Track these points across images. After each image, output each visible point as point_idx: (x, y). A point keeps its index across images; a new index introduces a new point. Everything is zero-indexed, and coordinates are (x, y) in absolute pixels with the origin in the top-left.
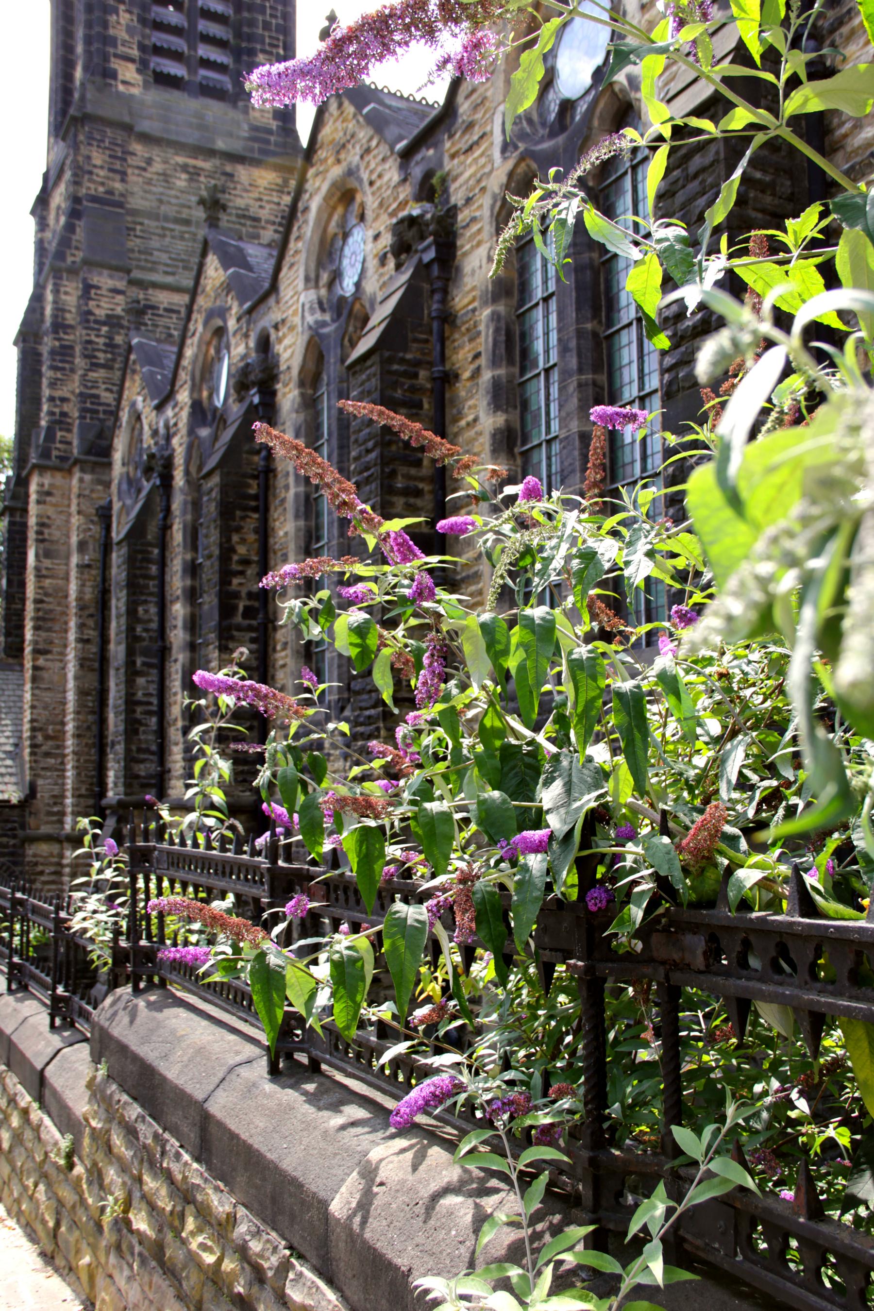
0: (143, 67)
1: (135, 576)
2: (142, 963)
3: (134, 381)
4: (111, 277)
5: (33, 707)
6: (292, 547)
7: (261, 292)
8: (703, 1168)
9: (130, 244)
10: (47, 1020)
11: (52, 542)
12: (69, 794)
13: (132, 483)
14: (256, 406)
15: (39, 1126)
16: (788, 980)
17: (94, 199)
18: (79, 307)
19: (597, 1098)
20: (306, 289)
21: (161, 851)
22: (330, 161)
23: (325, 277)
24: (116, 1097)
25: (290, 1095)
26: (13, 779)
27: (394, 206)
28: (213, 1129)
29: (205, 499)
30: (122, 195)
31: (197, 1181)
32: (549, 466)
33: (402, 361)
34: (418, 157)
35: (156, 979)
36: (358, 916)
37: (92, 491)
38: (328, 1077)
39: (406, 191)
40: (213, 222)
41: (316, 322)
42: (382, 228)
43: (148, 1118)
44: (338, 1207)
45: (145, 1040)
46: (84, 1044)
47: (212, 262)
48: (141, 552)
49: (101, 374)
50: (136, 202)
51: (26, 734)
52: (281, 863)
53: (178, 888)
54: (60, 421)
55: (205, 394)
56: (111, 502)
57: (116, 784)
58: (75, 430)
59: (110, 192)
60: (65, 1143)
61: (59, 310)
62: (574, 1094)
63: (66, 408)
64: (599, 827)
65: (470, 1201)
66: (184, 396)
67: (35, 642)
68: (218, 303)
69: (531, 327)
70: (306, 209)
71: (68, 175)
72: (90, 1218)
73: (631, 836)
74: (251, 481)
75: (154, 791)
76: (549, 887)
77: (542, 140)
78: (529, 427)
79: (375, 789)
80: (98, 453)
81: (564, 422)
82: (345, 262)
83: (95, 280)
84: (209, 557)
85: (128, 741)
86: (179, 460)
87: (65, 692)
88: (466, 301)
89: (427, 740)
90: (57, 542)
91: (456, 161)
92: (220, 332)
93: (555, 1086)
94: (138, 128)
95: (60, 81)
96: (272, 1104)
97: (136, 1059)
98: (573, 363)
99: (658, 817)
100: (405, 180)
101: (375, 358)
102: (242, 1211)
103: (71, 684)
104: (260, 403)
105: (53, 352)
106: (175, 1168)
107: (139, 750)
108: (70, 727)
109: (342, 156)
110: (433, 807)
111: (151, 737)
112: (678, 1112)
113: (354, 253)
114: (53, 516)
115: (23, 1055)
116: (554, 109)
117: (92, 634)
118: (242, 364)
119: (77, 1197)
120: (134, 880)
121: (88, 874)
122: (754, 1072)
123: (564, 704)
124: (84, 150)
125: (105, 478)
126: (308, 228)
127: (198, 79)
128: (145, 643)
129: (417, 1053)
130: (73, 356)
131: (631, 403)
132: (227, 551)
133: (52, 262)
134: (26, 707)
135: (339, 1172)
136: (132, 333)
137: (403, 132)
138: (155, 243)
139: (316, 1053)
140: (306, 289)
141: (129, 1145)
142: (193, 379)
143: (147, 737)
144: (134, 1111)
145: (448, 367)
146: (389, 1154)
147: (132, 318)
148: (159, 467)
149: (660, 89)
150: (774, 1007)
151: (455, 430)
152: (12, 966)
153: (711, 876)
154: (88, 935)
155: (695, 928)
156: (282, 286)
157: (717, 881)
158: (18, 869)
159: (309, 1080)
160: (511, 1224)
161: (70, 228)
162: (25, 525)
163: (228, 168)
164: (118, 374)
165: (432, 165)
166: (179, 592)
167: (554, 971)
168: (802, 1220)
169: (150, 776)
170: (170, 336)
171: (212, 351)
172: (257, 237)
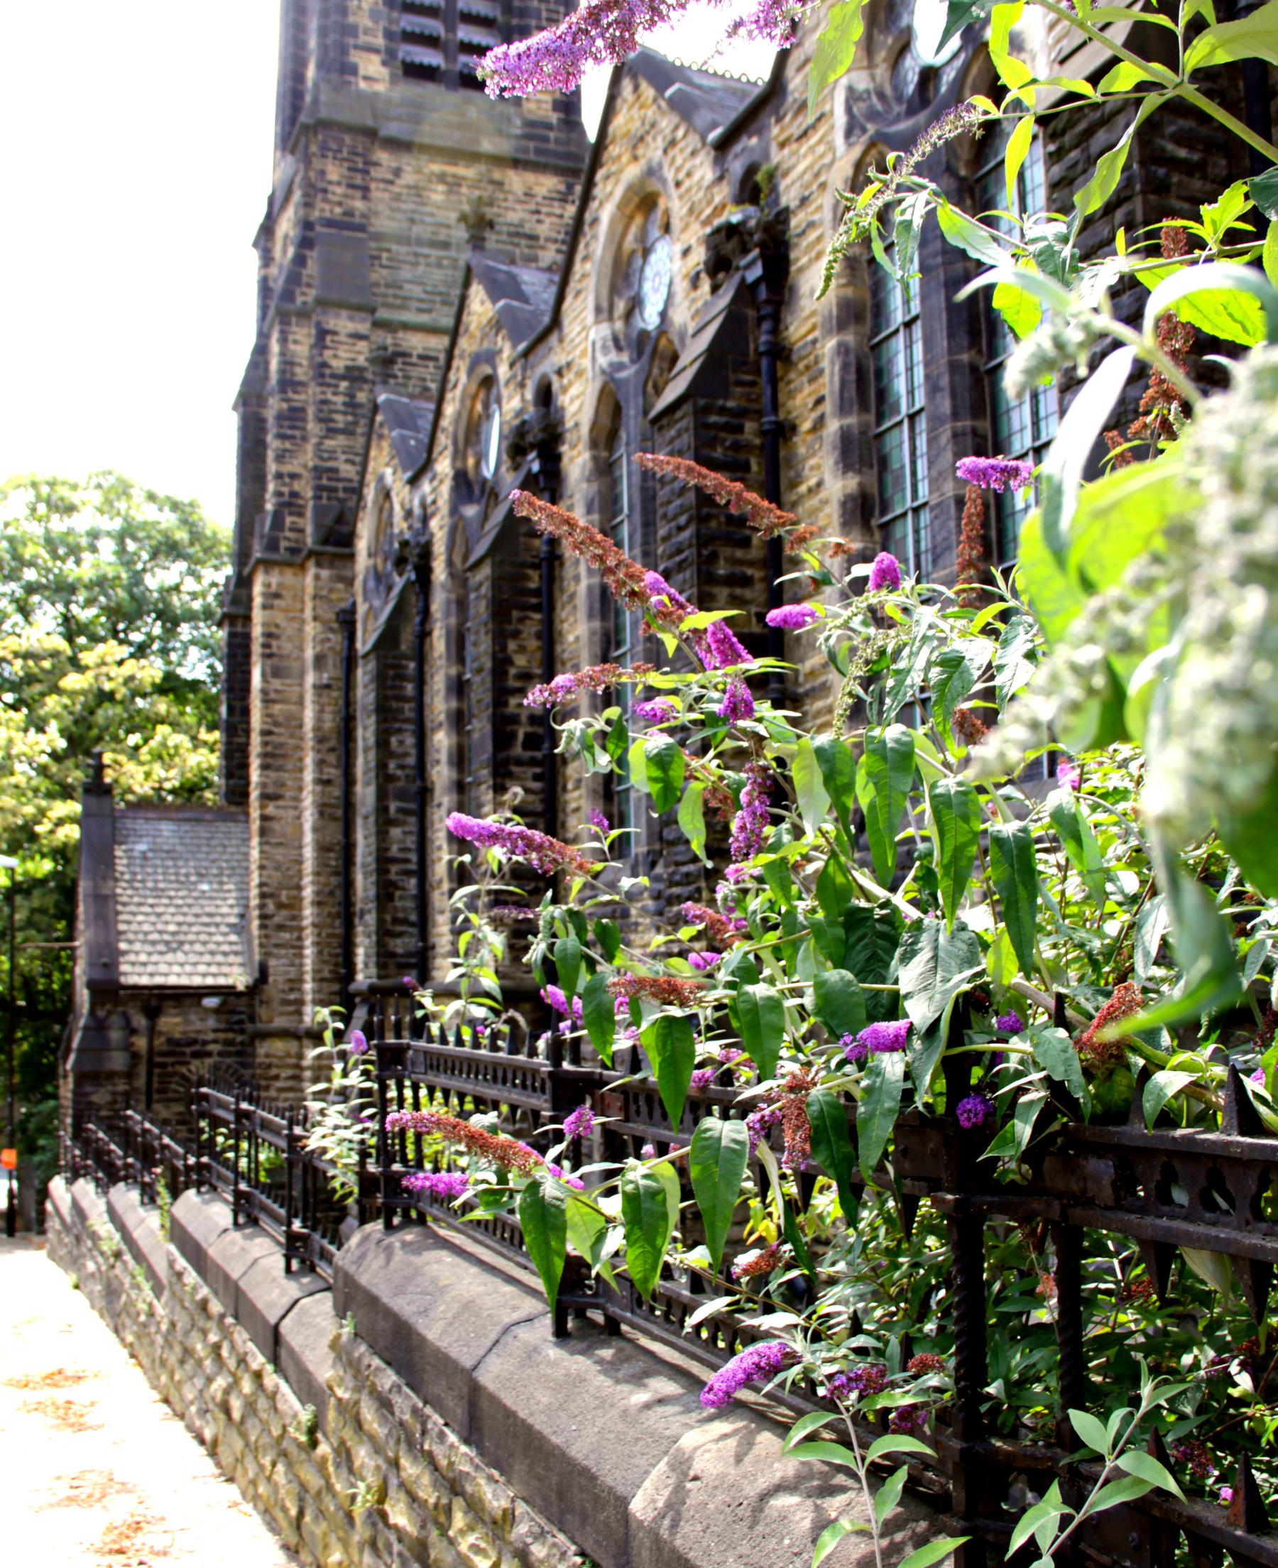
0: (389, 57)
1: (386, 698)
2: (391, 1193)
3: (380, 449)
4: (351, 319)
5: (262, 867)
6: (585, 654)
7: (540, 329)
8: (1109, 1464)
9: (374, 277)
10: (281, 1263)
11: (281, 657)
12: (308, 977)
13: (379, 577)
14: (536, 476)
15: (275, 1393)
16: (1224, 1219)
17: (330, 223)
18: (311, 358)
19: (972, 1373)
20: (597, 322)
21: (417, 1050)
22: (625, 159)
23: (621, 306)
24: (366, 1361)
25: (580, 1364)
26: (239, 959)
27: (708, 211)
28: (485, 1404)
29: (473, 596)
30: (364, 216)
31: (466, 1468)
32: (917, 542)
33: (723, 411)
34: (738, 148)
35: (414, 1214)
36: (664, 1133)
37: (331, 590)
38: (630, 1341)
39: (723, 193)
40: (477, 242)
41: (611, 365)
42: (693, 241)
43: (406, 1389)
44: (640, 1506)
45: (399, 1291)
46: (328, 1295)
47: (477, 294)
48: (395, 667)
49: (339, 442)
50: (384, 223)
51: (254, 902)
52: (566, 1065)
53: (438, 1095)
54: (290, 504)
55: (471, 462)
56: (354, 604)
57: (366, 965)
58: (309, 513)
59: (349, 213)
60: (306, 1415)
61: (288, 363)
62: (942, 1368)
63: (297, 486)
64: (974, 1017)
65: (809, 1502)
66: (444, 466)
67: (263, 785)
68: (486, 345)
69: (890, 361)
70: (595, 221)
71: (297, 196)
72: (339, 1507)
73: (1017, 1028)
74: (530, 572)
75: (414, 973)
76: (908, 1096)
77: (898, 119)
78: (889, 492)
79: (683, 970)
80: (337, 541)
81: (934, 483)
82: (647, 287)
83: (332, 323)
84: (479, 671)
85: (381, 909)
86: (439, 548)
87: (301, 847)
88: (803, 330)
89: (754, 904)
90: (288, 657)
91: (786, 151)
92: (488, 382)
93: (918, 1355)
94: (384, 132)
95: (289, 83)
96: (558, 1374)
97: (388, 1313)
98: (946, 405)
99: (1052, 1003)
100: (721, 179)
101: (687, 408)
102: (521, 1508)
103: (308, 837)
104: (541, 471)
105: (280, 417)
106: (438, 1451)
107: (396, 921)
108: (308, 893)
109: (640, 151)
110: (759, 990)
111: (410, 904)
112: (1077, 1392)
113: (657, 274)
114: (283, 624)
115: (253, 1307)
116: (912, 79)
117: (333, 772)
118: (517, 422)
119: (322, 1482)
120: (384, 1088)
121: (329, 1080)
122: (1183, 1337)
123: (929, 854)
124: (317, 164)
125: (348, 573)
126: (597, 244)
127: (458, 67)
128: (400, 784)
129: (742, 1311)
130: (304, 420)
131: (1022, 457)
132: (501, 663)
133: (279, 304)
134: (254, 867)
135: (642, 1461)
136: (378, 388)
137: (717, 118)
138: (406, 273)
139: (615, 1310)
140: (597, 322)
141: (383, 1420)
142: (455, 443)
143: (405, 904)
144: (388, 1379)
145: (782, 416)
146: (708, 1442)
147: (378, 369)
148: (414, 557)
149: (1051, 48)
150: (1206, 1255)
151: (793, 498)
152: (238, 1194)
153: (1122, 1083)
154: (328, 1157)
155: (1101, 1150)
156: (567, 319)
157: (1129, 1087)
158: (247, 1073)
159: (605, 1344)
160: (861, 1533)
161: (300, 260)
162: (247, 637)
163: (497, 175)
164: (361, 440)
165: (756, 157)
166: (442, 717)
167: (917, 1207)
168: (1239, 1533)
169: (409, 954)
170: (426, 389)
171: (479, 407)
172: (534, 259)
